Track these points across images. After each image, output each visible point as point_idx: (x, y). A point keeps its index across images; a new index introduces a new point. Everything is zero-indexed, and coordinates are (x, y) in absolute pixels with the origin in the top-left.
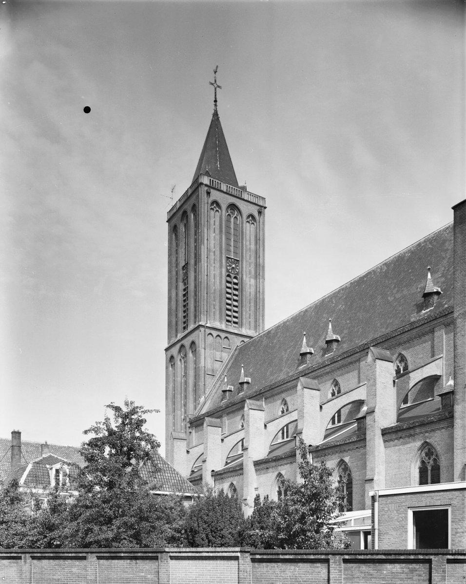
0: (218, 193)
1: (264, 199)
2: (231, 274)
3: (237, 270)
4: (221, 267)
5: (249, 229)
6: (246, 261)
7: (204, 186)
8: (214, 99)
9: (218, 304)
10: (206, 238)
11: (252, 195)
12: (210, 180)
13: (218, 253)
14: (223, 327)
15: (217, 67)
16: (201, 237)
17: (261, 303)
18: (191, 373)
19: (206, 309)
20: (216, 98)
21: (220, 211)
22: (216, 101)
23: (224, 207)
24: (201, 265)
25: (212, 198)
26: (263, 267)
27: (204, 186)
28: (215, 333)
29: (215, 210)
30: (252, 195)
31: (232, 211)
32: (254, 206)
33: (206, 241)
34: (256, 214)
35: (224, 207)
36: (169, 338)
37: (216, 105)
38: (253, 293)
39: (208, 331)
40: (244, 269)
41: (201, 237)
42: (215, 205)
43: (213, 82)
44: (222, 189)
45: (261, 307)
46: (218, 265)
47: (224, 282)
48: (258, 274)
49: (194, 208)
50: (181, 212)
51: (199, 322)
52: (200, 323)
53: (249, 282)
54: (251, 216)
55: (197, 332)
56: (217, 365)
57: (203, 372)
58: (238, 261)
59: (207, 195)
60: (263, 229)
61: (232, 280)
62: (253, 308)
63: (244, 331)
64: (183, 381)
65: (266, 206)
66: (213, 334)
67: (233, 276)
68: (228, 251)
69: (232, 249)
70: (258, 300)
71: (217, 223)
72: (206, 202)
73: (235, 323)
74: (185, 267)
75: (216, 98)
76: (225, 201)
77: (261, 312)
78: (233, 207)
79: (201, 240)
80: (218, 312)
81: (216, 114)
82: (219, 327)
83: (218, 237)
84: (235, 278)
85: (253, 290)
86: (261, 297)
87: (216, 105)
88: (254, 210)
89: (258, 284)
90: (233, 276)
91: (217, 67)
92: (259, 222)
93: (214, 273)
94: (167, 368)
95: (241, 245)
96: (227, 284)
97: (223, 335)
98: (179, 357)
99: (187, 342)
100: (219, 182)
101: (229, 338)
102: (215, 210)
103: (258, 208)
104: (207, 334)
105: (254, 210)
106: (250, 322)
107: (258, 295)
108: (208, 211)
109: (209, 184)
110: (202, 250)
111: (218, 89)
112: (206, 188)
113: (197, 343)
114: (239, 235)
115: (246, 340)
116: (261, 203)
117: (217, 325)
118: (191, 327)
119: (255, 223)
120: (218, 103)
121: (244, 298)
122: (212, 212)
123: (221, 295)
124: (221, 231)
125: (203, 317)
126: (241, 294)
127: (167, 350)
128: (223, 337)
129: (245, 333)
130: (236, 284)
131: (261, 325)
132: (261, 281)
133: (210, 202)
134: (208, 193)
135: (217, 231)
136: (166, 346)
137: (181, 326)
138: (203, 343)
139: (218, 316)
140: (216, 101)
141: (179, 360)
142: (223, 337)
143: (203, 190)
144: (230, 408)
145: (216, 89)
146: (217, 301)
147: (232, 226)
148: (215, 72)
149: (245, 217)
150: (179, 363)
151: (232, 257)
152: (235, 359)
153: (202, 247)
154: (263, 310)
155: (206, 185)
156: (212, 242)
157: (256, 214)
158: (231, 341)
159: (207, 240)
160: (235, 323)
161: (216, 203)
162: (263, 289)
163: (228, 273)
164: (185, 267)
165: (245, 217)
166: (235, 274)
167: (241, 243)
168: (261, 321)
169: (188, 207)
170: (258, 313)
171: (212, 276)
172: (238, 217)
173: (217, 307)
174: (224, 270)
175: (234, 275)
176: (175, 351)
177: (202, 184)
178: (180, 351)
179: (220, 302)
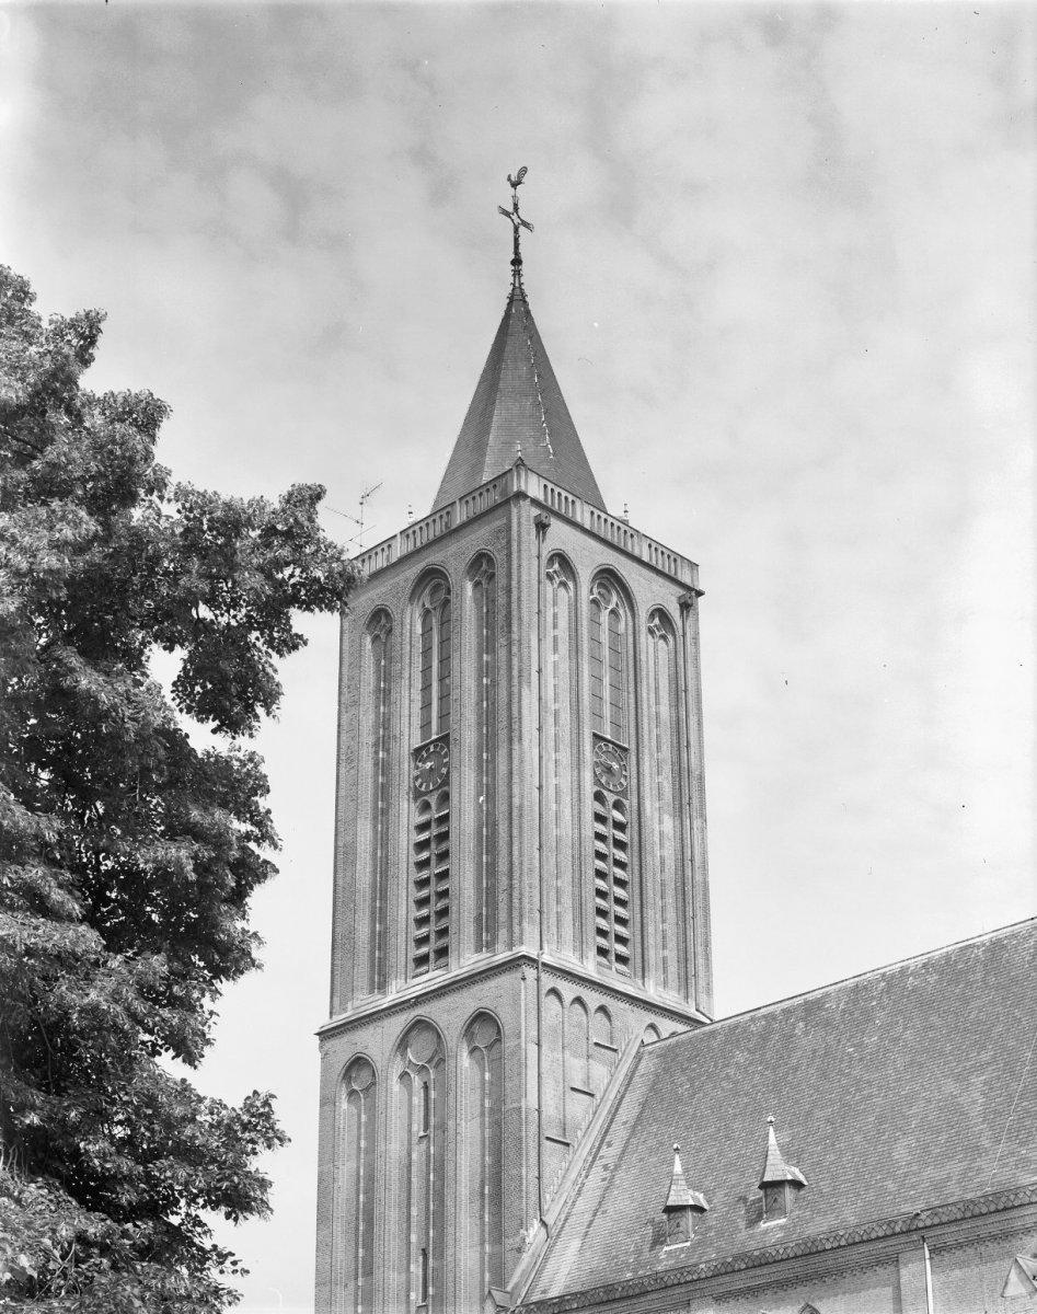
0: (567, 529)
1: (693, 566)
2: (605, 793)
3: (622, 780)
4: (578, 764)
5: (655, 653)
6: (651, 755)
7: (528, 502)
8: (513, 257)
9: (567, 890)
10: (535, 668)
11: (660, 549)
12: (545, 486)
13: (565, 717)
14: (590, 967)
15: (524, 171)
16: (521, 661)
17: (699, 898)
18: (469, 1133)
19: (537, 899)
20: (516, 252)
21: (571, 584)
22: (517, 262)
23: (585, 574)
24: (522, 752)
25: (549, 547)
26: (701, 778)
27: (528, 502)
28: (569, 990)
29: (557, 580)
30: (660, 549)
31: (603, 591)
32: (668, 584)
33: (535, 676)
34: (674, 610)
35: (585, 574)
36: (339, 989)
37: (517, 273)
38: (670, 864)
39: (549, 981)
40: (647, 781)
41: (521, 661)
42: (556, 566)
43: (511, 209)
44: (579, 519)
45: (699, 913)
46: (565, 756)
47: (588, 816)
48: (685, 800)
49: (482, 566)
50: (413, 571)
51: (511, 945)
52: (524, 950)
53: (660, 825)
54: (660, 613)
55: (505, 980)
56: (578, 1107)
57: (533, 1129)
58: (625, 750)
59: (538, 533)
60: (696, 659)
61: (609, 811)
62: (671, 915)
63: (652, 991)
64: (414, 1156)
65: (701, 587)
66: (563, 992)
67: (611, 798)
68: (597, 715)
69: (607, 711)
70: (688, 888)
71: (563, 623)
72: (535, 552)
73: (622, 959)
74: (437, 747)
75: (516, 252)
76: (588, 557)
77: (699, 931)
78: (608, 578)
79: (520, 671)
80: (568, 918)
81: (517, 299)
82: (578, 969)
83: (565, 667)
84: (618, 806)
85: (671, 852)
86: (698, 877)
87: (517, 273)
88: (669, 598)
89: (687, 835)
90: (611, 798)
91: (524, 171)
92: (684, 635)
93: (554, 782)
94: (327, 1102)
95: (632, 701)
96: (596, 825)
97: (594, 999)
98: (398, 1067)
99: (451, 1015)
100: (571, 498)
101: (610, 1009)
102: (557, 580)
103: (682, 592)
104: (544, 991)
105: (669, 598)
106: (664, 960)
107: (688, 872)
108: (539, 582)
109: (541, 498)
110: (525, 702)
111: (522, 229)
112: (535, 512)
113: (505, 1016)
114: (629, 669)
115: (667, 1026)
116: (685, 577)
117: (570, 961)
118: (467, 960)
119: (670, 637)
120: (524, 268)
121: (648, 876)
122: (549, 588)
123: (578, 860)
124: (576, 650)
125: (530, 931)
126: (636, 860)
127: (325, 1035)
128: (568, 996)
129: (656, 998)
130: (620, 826)
131: (701, 974)
132: (697, 823)
133: (545, 555)
134: (542, 527)
135: (564, 647)
136: (323, 1020)
137: (402, 949)
138: (535, 1021)
139: (568, 930)
140: (517, 262)
141: (395, 1078)
142: (568, 996)
143: (524, 514)
144: (737, 1276)
145: (516, 230)
146: (567, 877)
147: (605, 637)
148: (515, 185)
149: (643, 613)
150: (396, 1086)
151: (609, 737)
152: (653, 1088)
153: (525, 692)
154: (707, 924)
155: (535, 502)
156: (550, 681)
157: (674, 610)
158: (617, 1023)
159: (539, 671)
160: (622, 959)
161: (561, 559)
162: (704, 853)
163: (596, 788)
164: (437, 747)
165: (643, 613)
166: (617, 793)
167: (632, 696)
168: (700, 961)
169: (454, 559)
170: (690, 933)
171: (552, 792)
172: (621, 611)
173: (567, 901)
174: (588, 776)
175: (616, 797)
176: (377, 1042)
177: (521, 495)
178: (403, 1044)
179: (578, 883)
